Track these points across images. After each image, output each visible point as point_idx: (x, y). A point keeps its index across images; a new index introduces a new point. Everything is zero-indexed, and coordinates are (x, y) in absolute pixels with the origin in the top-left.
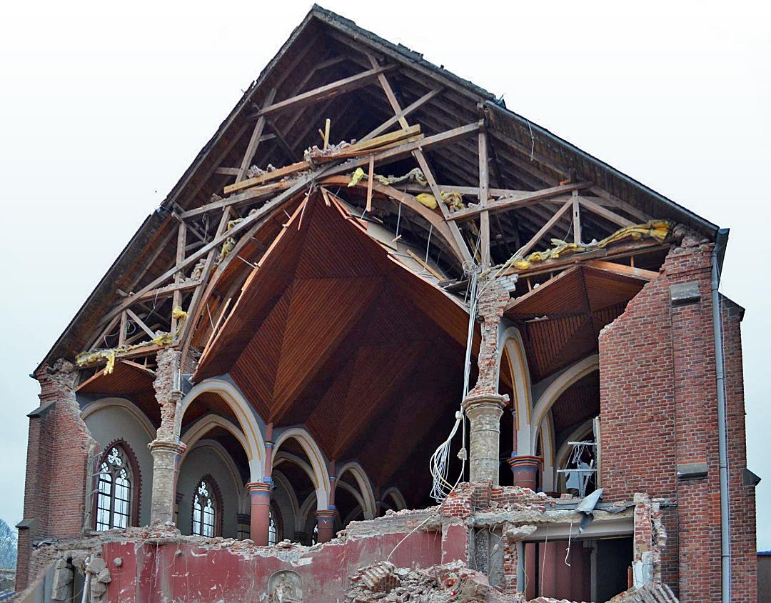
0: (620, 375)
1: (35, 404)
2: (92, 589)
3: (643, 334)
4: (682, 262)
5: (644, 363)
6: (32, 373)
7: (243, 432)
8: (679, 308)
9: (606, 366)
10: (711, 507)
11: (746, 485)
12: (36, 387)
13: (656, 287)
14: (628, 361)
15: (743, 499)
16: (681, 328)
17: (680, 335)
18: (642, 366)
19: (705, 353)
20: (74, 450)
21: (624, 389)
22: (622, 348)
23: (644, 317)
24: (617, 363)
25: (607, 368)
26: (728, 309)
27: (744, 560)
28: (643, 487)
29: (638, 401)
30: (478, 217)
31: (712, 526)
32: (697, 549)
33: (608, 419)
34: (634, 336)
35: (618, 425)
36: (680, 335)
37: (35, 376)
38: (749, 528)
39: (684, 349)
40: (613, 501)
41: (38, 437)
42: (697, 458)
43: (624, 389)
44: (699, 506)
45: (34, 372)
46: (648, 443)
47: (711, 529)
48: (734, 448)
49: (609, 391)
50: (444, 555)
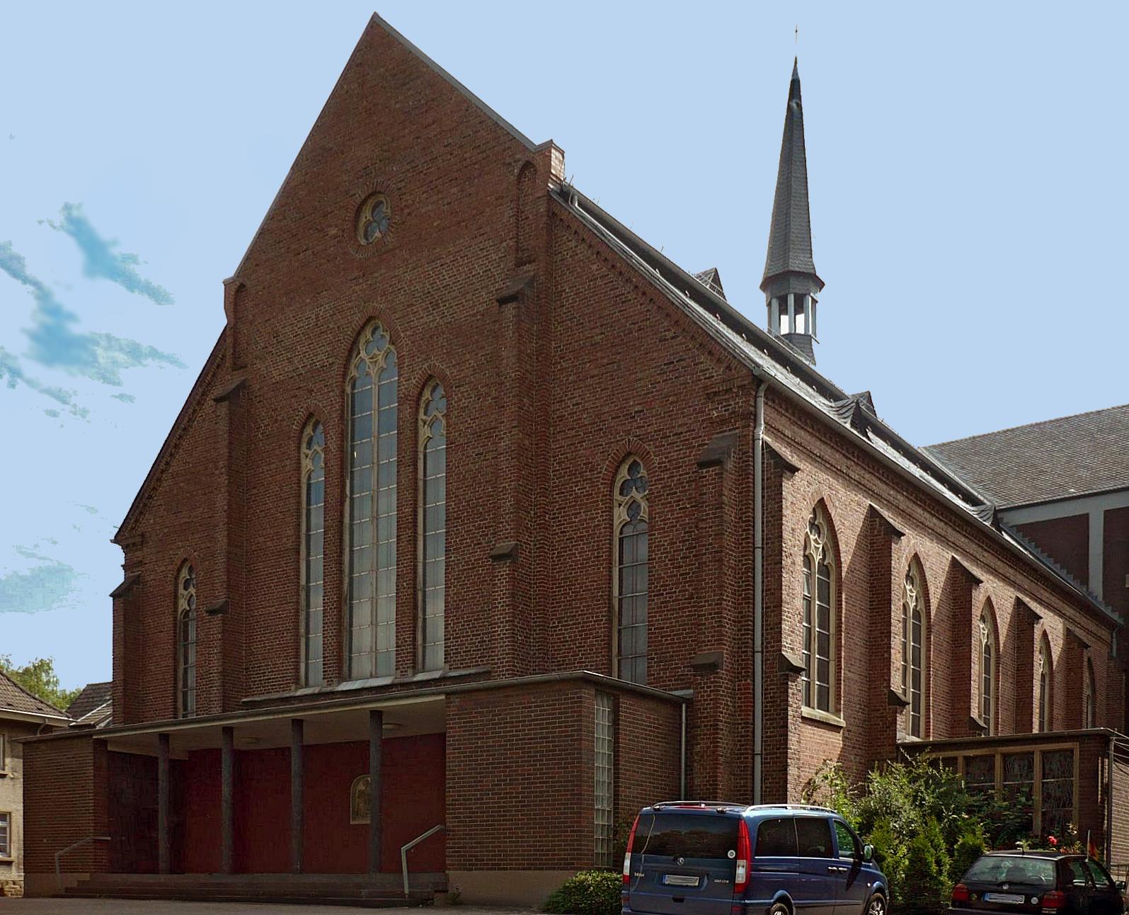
0: (666, 544)
2: (751, 717)
3: (687, 494)
4: (725, 406)
7: (796, 63)
8: (704, 471)
11: (780, 671)
12: (118, 548)
15: (778, 688)
17: (704, 502)
18: (685, 533)
19: (740, 518)
24: (664, 529)
27: (777, 758)
28: (683, 675)
29: (681, 575)
31: (742, 719)
32: (708, 748)
35: (662, 603)
36: (704, 502)
38: (782, 721)
41: (122, 622)
42: (714, 645)
44: (711, 700)
45: (115, 537)
46: (688, 624)
47: (741, 724)
50: (366, 770)
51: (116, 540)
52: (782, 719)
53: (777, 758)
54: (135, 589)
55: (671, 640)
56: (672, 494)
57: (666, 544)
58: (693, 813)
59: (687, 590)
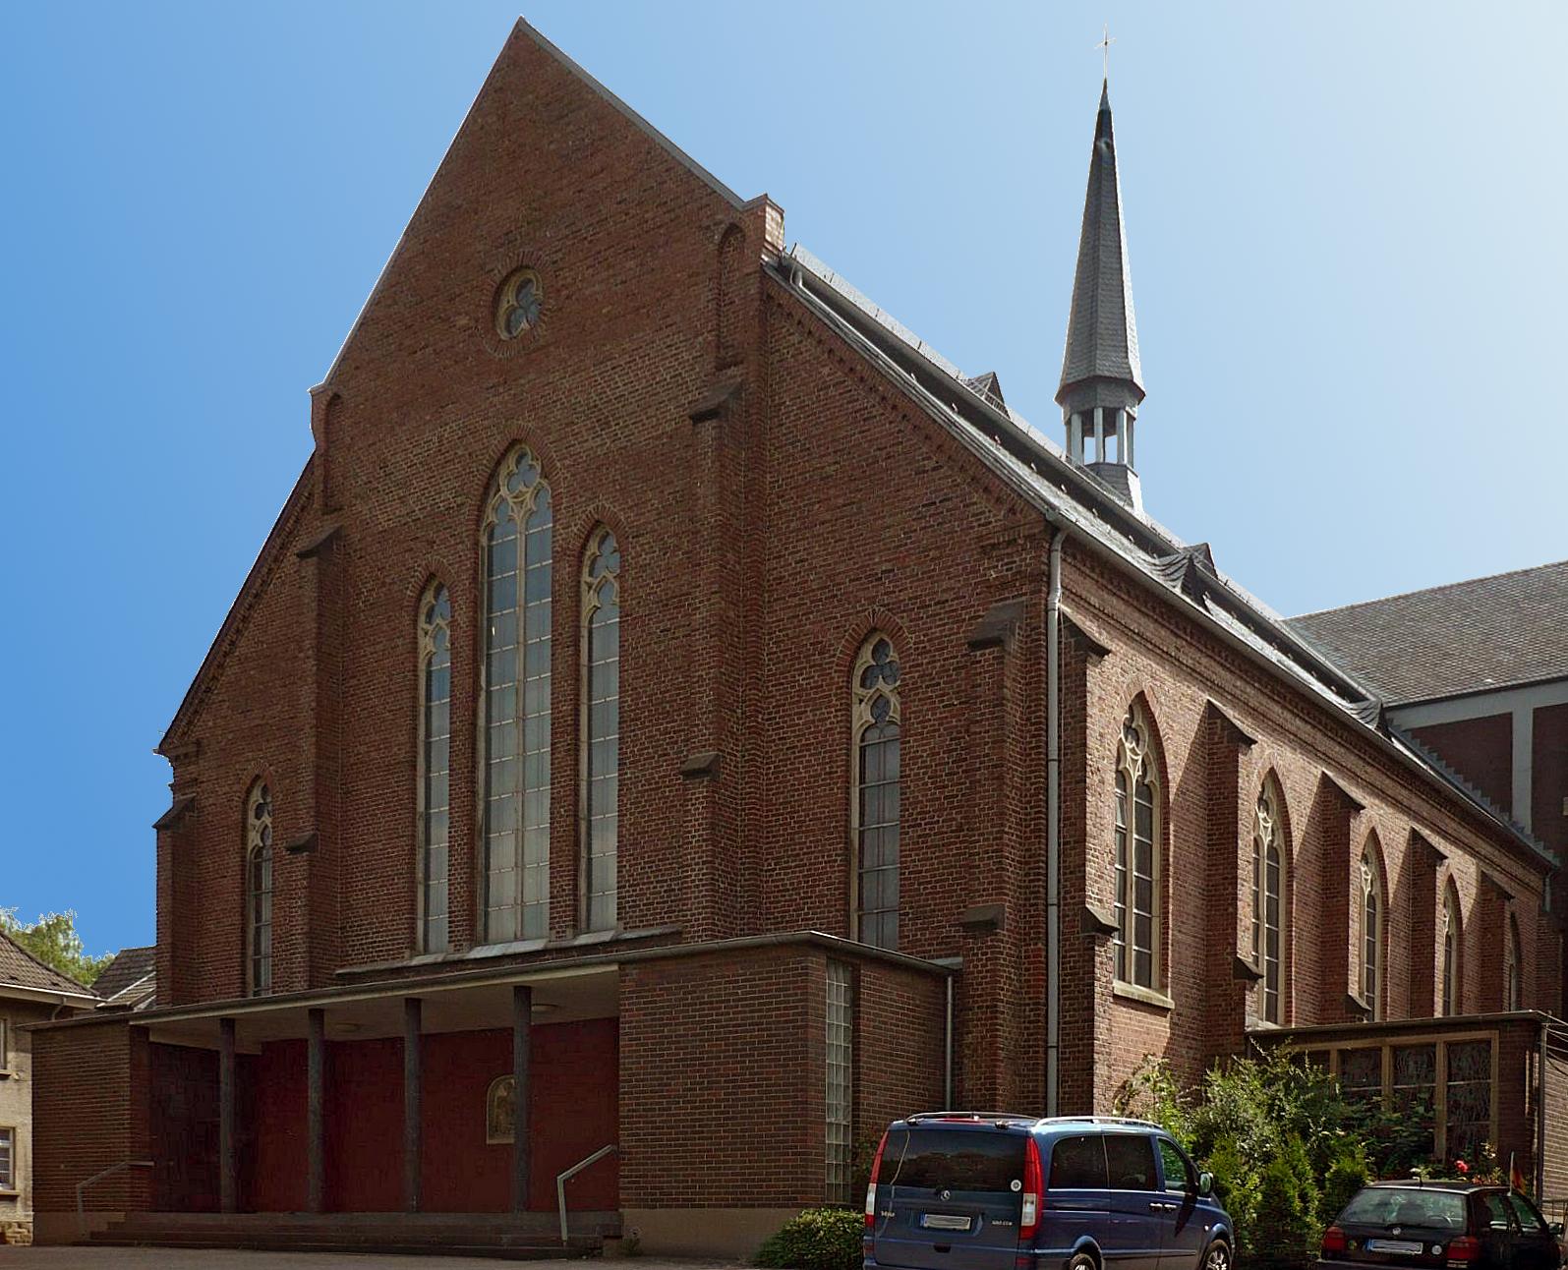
0: (925, 755)
1: (165, 802)
2: (1044, 996)
4: (1006, 564)
5: (954, 735)
6: (157, 747)
8: (978, 653)
9: (908, 739)
10: (1029, 970)
13: (973, 606)
14: (935, 731)
16: (980, 685)
17: (977, 697)
19: (1028, 719)
20: (225, 881)
21: (929, 778)
22: (928, 710)
23: (957, 657)
24: (922, 734)
25: (909, 742)
26: (1072, 640)
30: (1085, 428)
31: (1030, 999)
33: (909, 827)
34: (944, 689)
35: (919, 836)
36: (977, 697)
37: (161, 750)
39: (982, 720)
40: (1333, 897)
41: (170, 864)
43: (929, 778)
47: (1029, 1005)
48: (1071, 873)
49: (911, 781)
51: (161, 750)
52: (1086, 997)
53: (1079, 1052)
54: (187, 818)
55: (931, 888)
56: (934, 685)
57: (925, 755)
58: (962, 1128)
59: (954, 819)
